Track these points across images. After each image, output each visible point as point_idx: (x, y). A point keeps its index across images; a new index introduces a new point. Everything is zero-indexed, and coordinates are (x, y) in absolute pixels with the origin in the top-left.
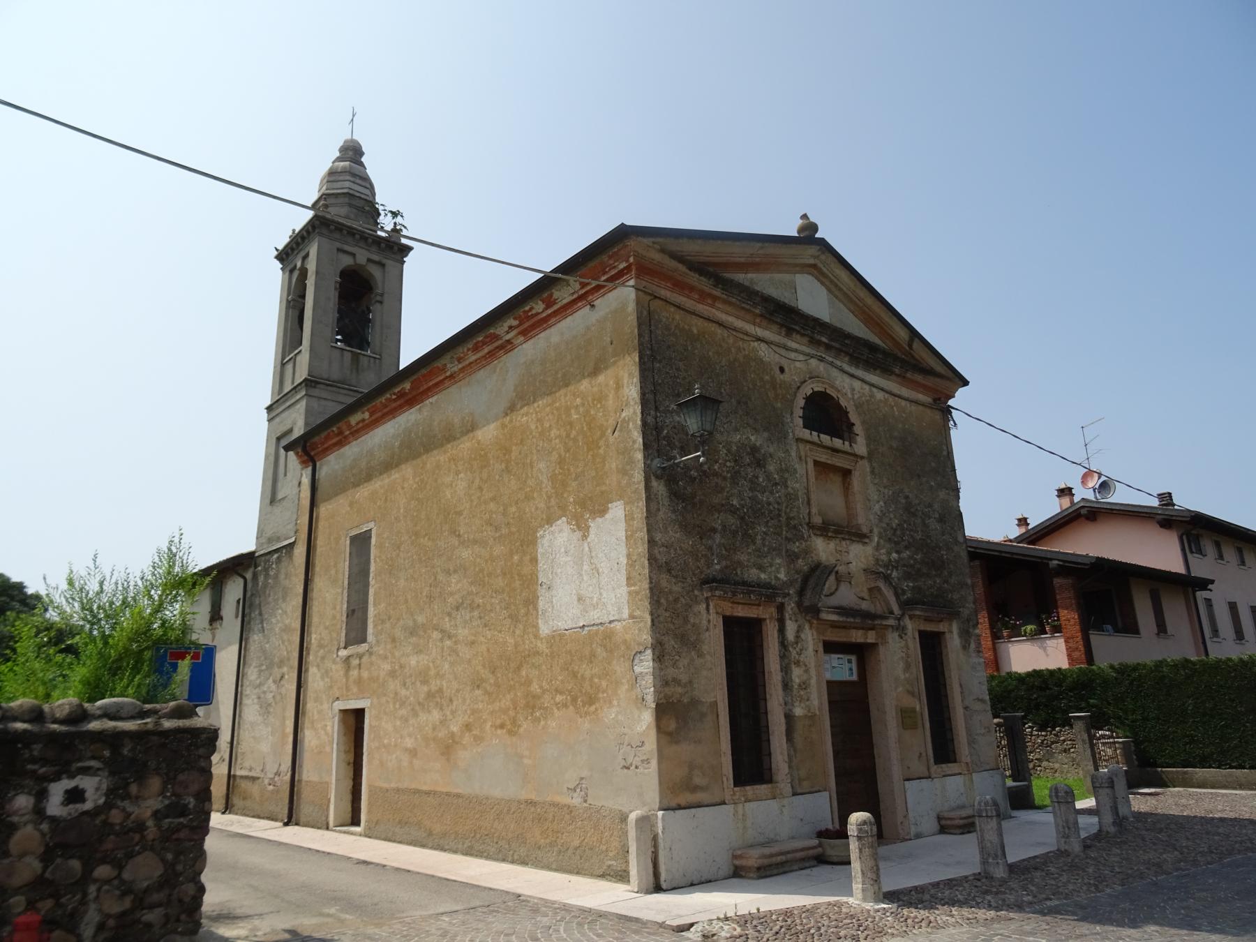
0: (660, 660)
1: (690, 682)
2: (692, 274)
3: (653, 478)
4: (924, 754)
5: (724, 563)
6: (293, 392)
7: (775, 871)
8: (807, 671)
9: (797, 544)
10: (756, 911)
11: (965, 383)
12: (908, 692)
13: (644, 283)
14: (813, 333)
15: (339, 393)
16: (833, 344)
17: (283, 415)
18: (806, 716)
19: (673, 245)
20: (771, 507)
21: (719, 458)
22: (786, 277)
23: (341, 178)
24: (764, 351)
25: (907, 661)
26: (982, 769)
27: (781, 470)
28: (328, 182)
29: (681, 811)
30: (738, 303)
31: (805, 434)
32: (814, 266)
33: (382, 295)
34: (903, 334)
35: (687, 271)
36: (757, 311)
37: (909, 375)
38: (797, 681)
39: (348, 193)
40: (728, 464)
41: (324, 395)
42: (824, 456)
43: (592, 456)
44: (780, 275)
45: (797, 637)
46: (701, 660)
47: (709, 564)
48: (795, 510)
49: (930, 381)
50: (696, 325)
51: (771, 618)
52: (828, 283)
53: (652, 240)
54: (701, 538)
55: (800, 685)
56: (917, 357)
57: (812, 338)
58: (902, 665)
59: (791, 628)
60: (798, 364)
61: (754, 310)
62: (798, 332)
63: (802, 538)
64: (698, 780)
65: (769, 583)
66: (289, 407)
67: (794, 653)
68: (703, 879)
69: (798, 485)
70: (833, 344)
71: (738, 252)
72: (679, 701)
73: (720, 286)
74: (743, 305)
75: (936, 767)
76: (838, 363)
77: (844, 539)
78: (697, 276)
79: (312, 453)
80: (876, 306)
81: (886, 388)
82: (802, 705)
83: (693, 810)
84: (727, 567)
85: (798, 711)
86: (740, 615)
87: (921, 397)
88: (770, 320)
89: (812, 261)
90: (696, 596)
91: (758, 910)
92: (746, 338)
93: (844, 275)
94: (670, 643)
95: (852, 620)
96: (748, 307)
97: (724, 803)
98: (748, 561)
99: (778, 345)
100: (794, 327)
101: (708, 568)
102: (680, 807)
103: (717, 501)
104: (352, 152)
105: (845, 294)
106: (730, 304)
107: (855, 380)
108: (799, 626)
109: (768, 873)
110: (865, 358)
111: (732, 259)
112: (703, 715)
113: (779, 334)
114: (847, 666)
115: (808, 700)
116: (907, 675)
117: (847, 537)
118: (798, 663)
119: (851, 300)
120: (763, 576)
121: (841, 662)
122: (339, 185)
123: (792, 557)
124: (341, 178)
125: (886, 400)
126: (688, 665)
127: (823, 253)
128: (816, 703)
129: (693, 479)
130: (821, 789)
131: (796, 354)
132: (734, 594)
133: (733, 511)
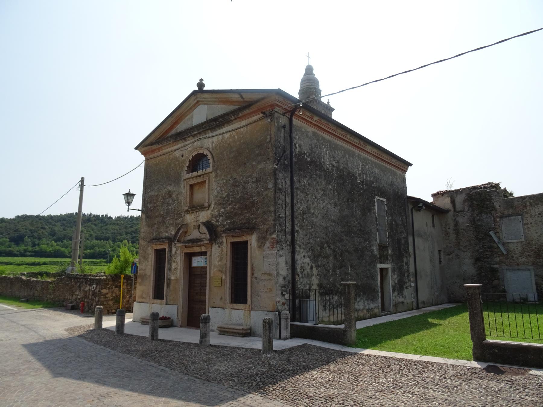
1: (145, 269)
2: (152, 146)
5: (156, 233)
7: (146, 324)
8: (177, 264)
9: (179, 220)
12: (219, 270)
16: (200, 131)
18: (175, 280)
19: (147, 142)
24: (177, 154)
25: (221, 257)
26: (262, 310)
32: (198, 102)
34: (236, 96)
37: (240, 115)
38: (174, 268)
45: (176, 253)
47: (153, 235)
49: (254, 108)
55: (174, 269)
58: (218, 259)
60: (189, 149)
62: (187, 138)
64: (144, 296)
67: (174, 258)
70: (200, 131)
71: (167, 126)
75: (229, 304)
76: (207, 135)
77: (197, 212)
81: (229, 130)
82: (174, 276)
85: (173, 278)
86: (159, 248)
87: (255, 118)
89: (196, 101)
94: (142, 259)
95: (188, 244)
97: (148, 303)
99: (184, 146)
100: (184, 137)
104: (309, 70)
105: (212, 101)
108: (177, 249)
113: (183, 142)
114: (204, 260)
117: (198, 211)
118: (174, 262)
119: (215, 101)
120: (167, 234)
121: (201, 259)
125: (231, 135)
131: (188, 146)
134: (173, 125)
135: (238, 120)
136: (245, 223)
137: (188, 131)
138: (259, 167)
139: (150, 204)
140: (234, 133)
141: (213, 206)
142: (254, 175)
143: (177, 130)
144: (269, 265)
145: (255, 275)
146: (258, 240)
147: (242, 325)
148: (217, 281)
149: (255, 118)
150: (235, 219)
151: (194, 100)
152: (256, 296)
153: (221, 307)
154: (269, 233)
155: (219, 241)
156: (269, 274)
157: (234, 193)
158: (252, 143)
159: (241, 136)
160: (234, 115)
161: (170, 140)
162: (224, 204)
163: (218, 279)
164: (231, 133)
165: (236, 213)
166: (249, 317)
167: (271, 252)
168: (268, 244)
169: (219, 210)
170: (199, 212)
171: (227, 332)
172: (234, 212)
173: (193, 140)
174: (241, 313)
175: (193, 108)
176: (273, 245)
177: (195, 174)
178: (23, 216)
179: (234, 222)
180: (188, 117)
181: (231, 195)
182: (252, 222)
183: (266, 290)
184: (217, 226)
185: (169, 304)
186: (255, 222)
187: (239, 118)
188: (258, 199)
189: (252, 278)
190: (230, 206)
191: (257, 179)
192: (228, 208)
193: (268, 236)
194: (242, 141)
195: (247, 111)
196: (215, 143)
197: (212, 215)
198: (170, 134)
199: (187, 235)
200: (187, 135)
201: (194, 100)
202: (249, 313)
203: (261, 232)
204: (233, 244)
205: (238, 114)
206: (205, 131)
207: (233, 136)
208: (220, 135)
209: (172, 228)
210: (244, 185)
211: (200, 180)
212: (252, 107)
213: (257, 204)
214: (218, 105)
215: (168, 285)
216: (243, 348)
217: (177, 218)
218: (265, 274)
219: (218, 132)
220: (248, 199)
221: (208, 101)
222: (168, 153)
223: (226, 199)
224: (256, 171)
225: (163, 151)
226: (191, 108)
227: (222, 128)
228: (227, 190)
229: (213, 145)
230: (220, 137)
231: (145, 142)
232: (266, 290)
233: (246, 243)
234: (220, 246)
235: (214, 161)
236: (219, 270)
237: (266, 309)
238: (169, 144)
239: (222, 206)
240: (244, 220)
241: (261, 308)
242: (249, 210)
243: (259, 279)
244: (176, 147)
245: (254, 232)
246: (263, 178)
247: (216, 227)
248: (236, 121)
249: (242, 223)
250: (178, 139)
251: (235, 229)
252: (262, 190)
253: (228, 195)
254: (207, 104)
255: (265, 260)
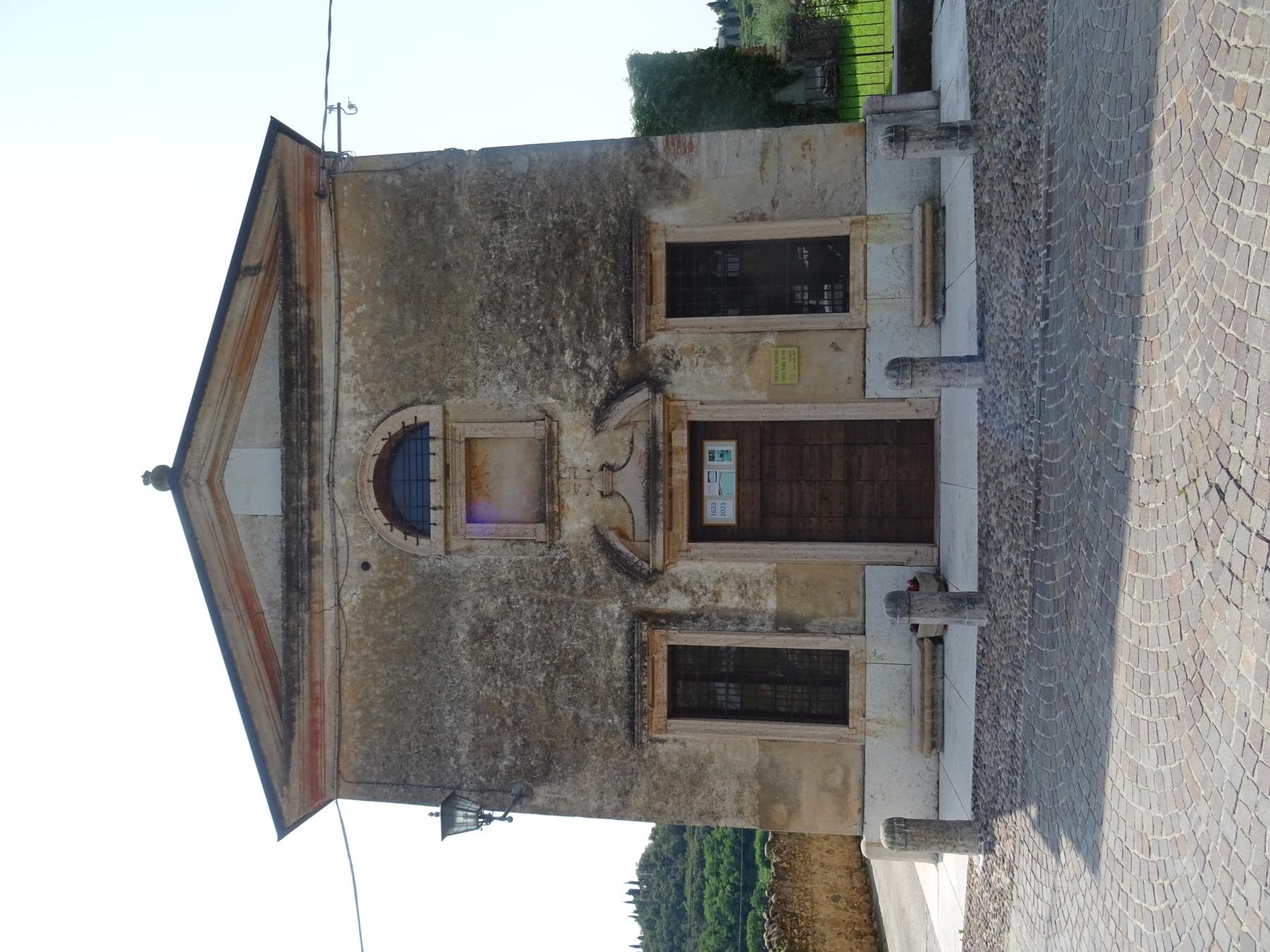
0: (718, 818)
2: (296, 731)
3: (533, 803)
4: (833, 337)
5: (611, 708)
7: (940, 662)
9: (575, 573)
10: (962, 934)
11: (277, 130)
13: (328, 786)
14: (302, 509)
16: (305, 465)
19: (275, 762)
20: (538, 615)
21: (495, 698)
22: (242, 531)
24: (352, 598)
27: (490, 589)
29: (866, 809)
30: (306, 651)
31: (436, 533)
34: (246, 290)
35: (296, 736)
36: (306, 617)
38: (737, 599)
40: (499, 683)
42: (458, 499)
44: (245, 551)
46: (716, 759)
48: (535, 571)
50: (352, 713)
51: (667, 638)
52: (223, 449)
53: (281, 800)
54: (587, 740)
56: (268, 249)
57: (309, 509)
58: (714, 370)
59: (678, 602)
60: (351, 532)
61: (307, 623)
62: (310, 536)
63: (566, 560)
64: (836, 780)
65: (627, 632)
68: (935, 793)
69: (504, 561)
70: (305, 465)
71: (246, 646)
72: (758, 795)
73: (296, 686)
74: (307, 643)
76: (326, 441)
77: (559, 478)
78: (296, 723)
80: (223, 359)
83: (867, 797)
84: (615, 705)
85: (771, 604)
87: (325, 233)
88: (311, 590)
89: (205, 490)
90: (650, 757)
91: (961, 932)
92: (343, 628)
93: (202, 430)
95: (661, 500)
96: (306, 633)
97: (863, 748)
98: (604, 666)
100: (306, 547)
101: (617, 733)
102: (862, 811)
103: (543, 707)
105: (226, 417)
106: (311, 659)
107: (340, 410)
109: (940, 733)
110: (305, 391)
111: (256, 653)
112: (773, 764)
115: (758, 582)
116: (728, 359)
120: (619, 644)
121: (712, 476)
123: (593, 589)
126: (722, 778)
127: (187, 476)
128: (762, 567)
129: (526, 744)
130: (862, 575)
131: (339, 536)
132: (644, 713)
133: (551, 684)
134: (251, 618)
135: (314, 297)
136: (616, 257)
137: (293, 517)
138: (465, 208)
139: (503, 757)
140: (348, 319)
141: (550, 400)
142: (484, 226)
143: (270, 603)
144: (737, 155)
145: (766, 206)
146: (667, 198)
147: (911, 246)
148: (784, 365)
149: (325, 233)
150: (600, 296)
151: (200, 495)
152: (826, 200)
153: (862, 341)
154: (649, 162)
155: (660, 365)
156: (764, 153)
157: (524, 305)
158: (393, 242)
159: (364, 287)
160: (297, 305)
161: (300, 622)
162: (550, 352)
163: (776, 361)
164: (345, 330)
165: (582, 299)
166: (884, 222)
167: (703, 151)
168: (680, 165)
169: (566, 372)
170: (562, 466)
171: (935, 275)
172: (578, 303)
173: (328, 568)
174: (877, 253)
175: (224, 512)
176: (684, 144)
177: (436, 516)
178: (447, 150)
179: (609, 302)
180: (245, 545)
181: (528, 319)
182: (613, 226)
183: (808, 161)
184: (615, 374)
185: (860, 618)
186: (615, 215)
187: (308, 290)
188: (554, 208)
189: (773, 219)
190: (560, 323)
191: (495, 218)
192: (565, 329)
193: (660, 164)
194: (378, 283)
195: (299, 250)
196: (359, 401)
197: (578, 401)
198: (279, 650)
199: (629, 533)
200: (302, 530)
201: (200, 495)
202: (875, 222)
203: (646, 190)
204: (672, 312)
205: (298, 288)
206: (310, 442)
207: (355, 321)
208: (338, 380)
209: (599, 614)
210: (504, 268)
211: (459, 452)
212: (292, 228)
213: (566, 212)
214: (246, 392)
215: (796, 626)
216: (970, 36)
217: (566, 586)
218: (762, 168)
219: (327, 391)
220: (548, 249)
221: (222, 435)
222: (339, 648)
223: (535, 341)
224: (473, 220)
225: (326, 680)
226: (222, 520)
227: (320, 370)
228: (511, 338)
229: (362, 413)
230: (345, 377)
231: (272, 772)
232: (808, 161)
233: (676, 252)
234: (675, 359)
235: (416, 402)
236: (750, 360)
237: (861, 159)
238: (310, 632)
239: (554, 358)
240: (605, 261)
241: (857, 178)
242: (580, 242)
243: (776, 191)
244: (329, 602)
245: (646, 215)
246: (498, 196)
247: (614, 383)
248: (314, 305)
249: (614, 267)
250: (306, 577)
251: (629, 297)
252: (531, 196)
253: (526, 332)
254: (231, 442)
255: (723, 172)
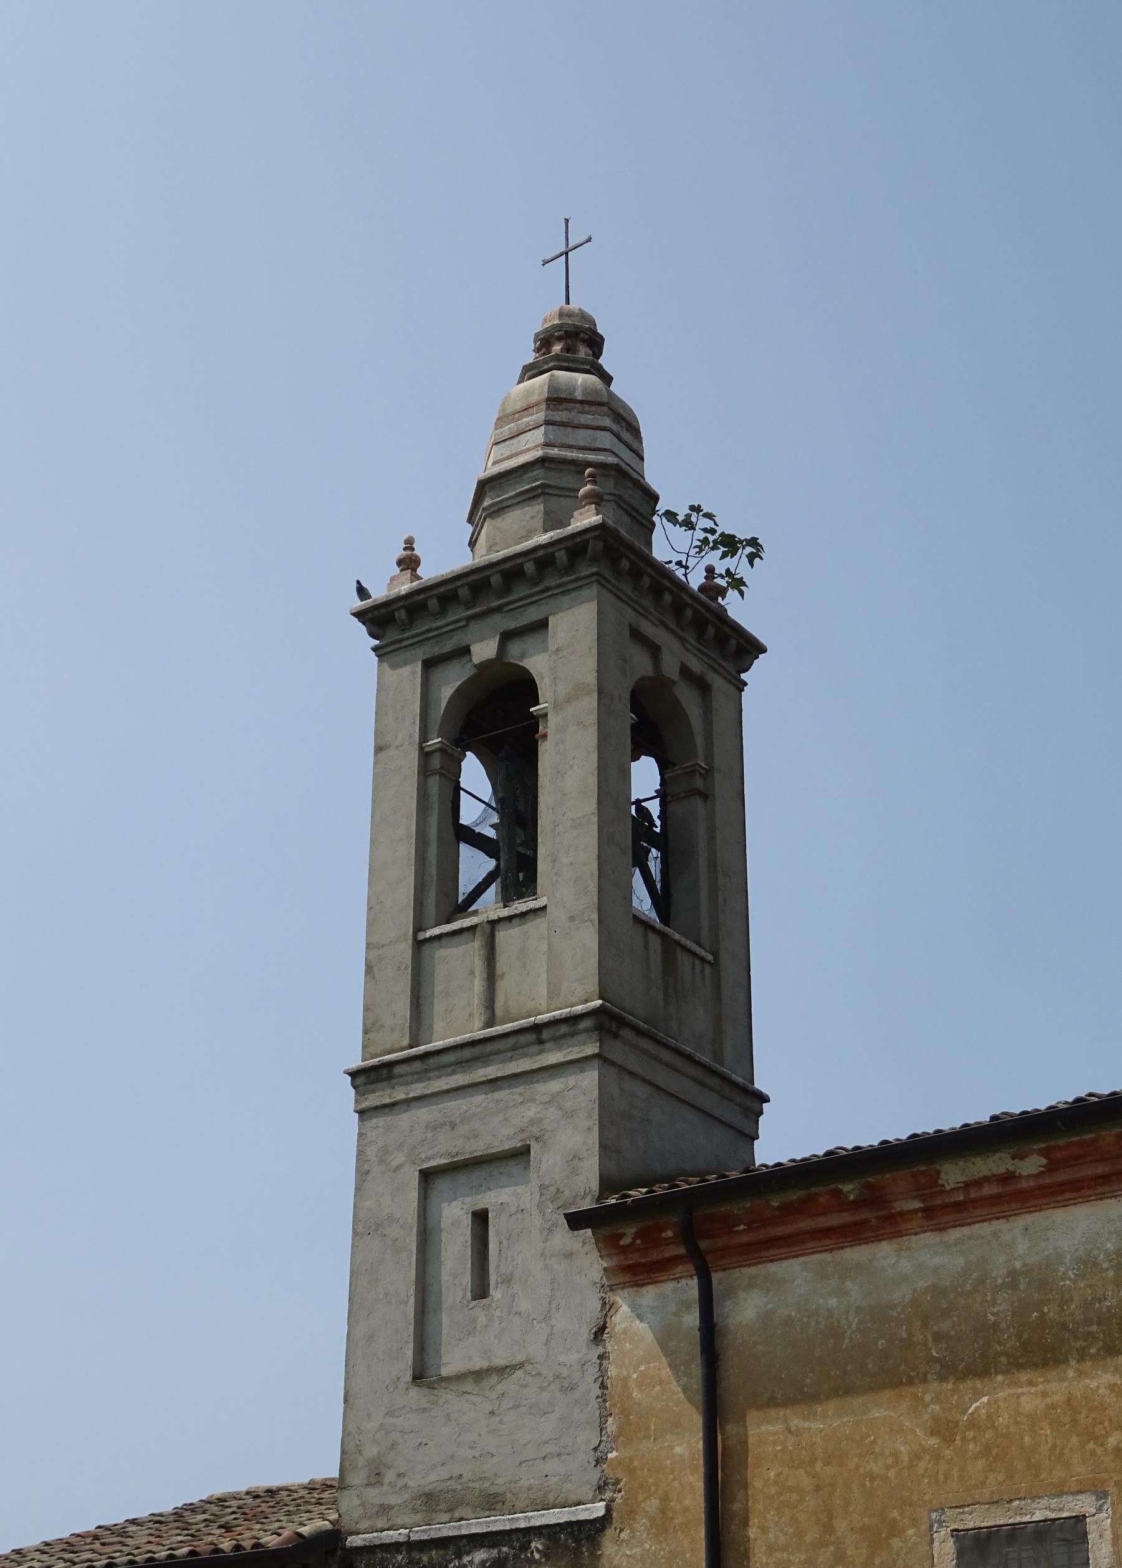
6: (564, 1029)
15: (657, 1059)
17: (455, 1106)
23: (587, 419)
28: (547, 423)
33: (708, 774)
39: (616, 468)
41: (633, 1062)
43: (1094, 1419)
66: (494, 1083)
79: (704, 1245)
122: (582, 437)
124: (587, 419)
